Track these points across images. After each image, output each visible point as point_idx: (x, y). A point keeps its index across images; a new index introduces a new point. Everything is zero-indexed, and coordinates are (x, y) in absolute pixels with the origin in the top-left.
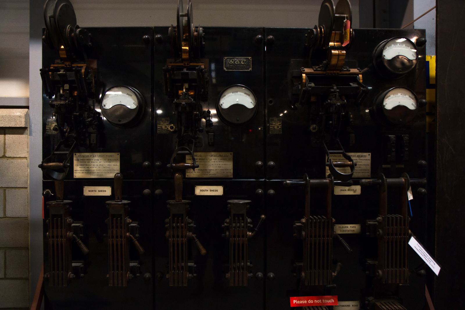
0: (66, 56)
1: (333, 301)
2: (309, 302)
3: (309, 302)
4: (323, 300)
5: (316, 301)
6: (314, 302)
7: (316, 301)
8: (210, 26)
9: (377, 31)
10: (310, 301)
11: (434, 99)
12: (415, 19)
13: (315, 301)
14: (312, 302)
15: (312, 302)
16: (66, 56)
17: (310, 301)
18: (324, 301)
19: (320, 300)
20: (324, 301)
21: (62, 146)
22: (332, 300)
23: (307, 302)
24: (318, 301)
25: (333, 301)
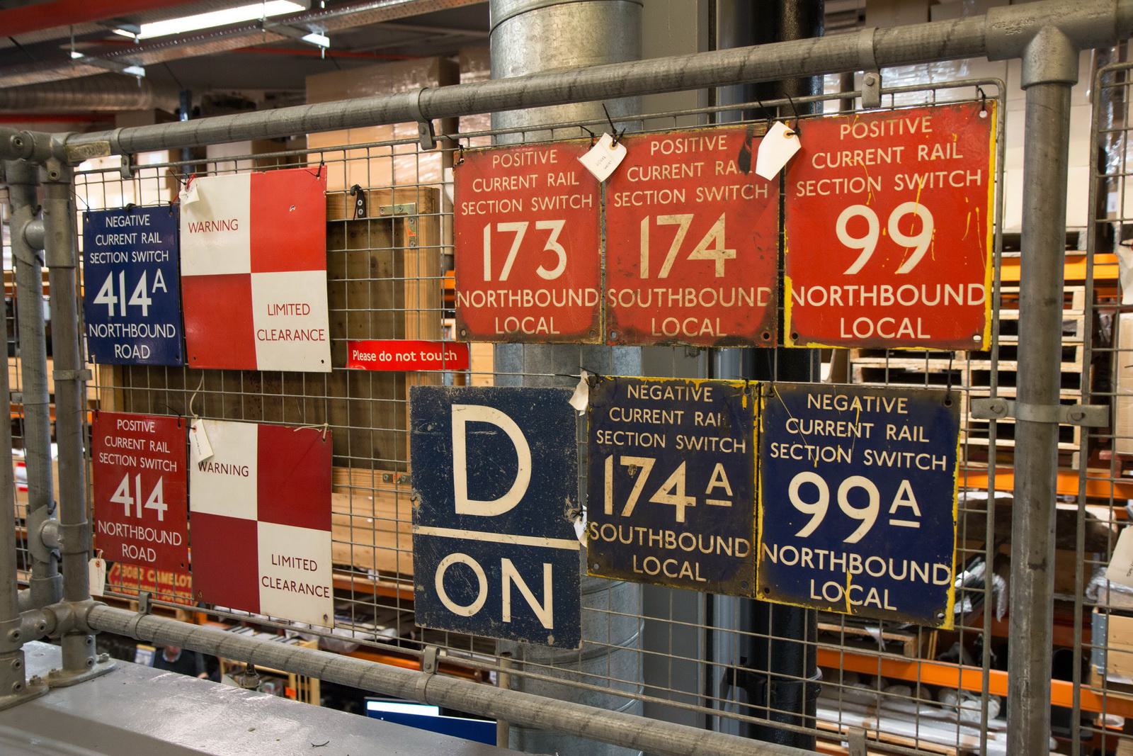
0: (1093, 50)
1: (453, 356)
2: (382, 357)
3: (382, 357)
4: (422, 354)
5: (399, 357)
6: (394, 357)
7: (399, 357)
8: (212, 51)
9: (977, 338)
10: (383, 354)
11: (245, 148)
12: (13, 44)
13: (397, 355)
14: (389, 357)
15: (389, 357)
16: (1093, 50)
17: (383, 354)
18: (425, 357)
19: (413, 354)
20: (425, 357)
21: (632, 473)
22: (451, 354)
23: (378, 358)
24: (407, 357)
25: (453, 356)
